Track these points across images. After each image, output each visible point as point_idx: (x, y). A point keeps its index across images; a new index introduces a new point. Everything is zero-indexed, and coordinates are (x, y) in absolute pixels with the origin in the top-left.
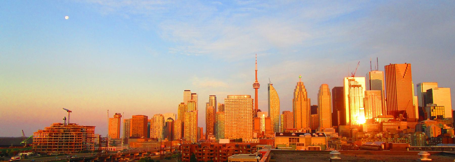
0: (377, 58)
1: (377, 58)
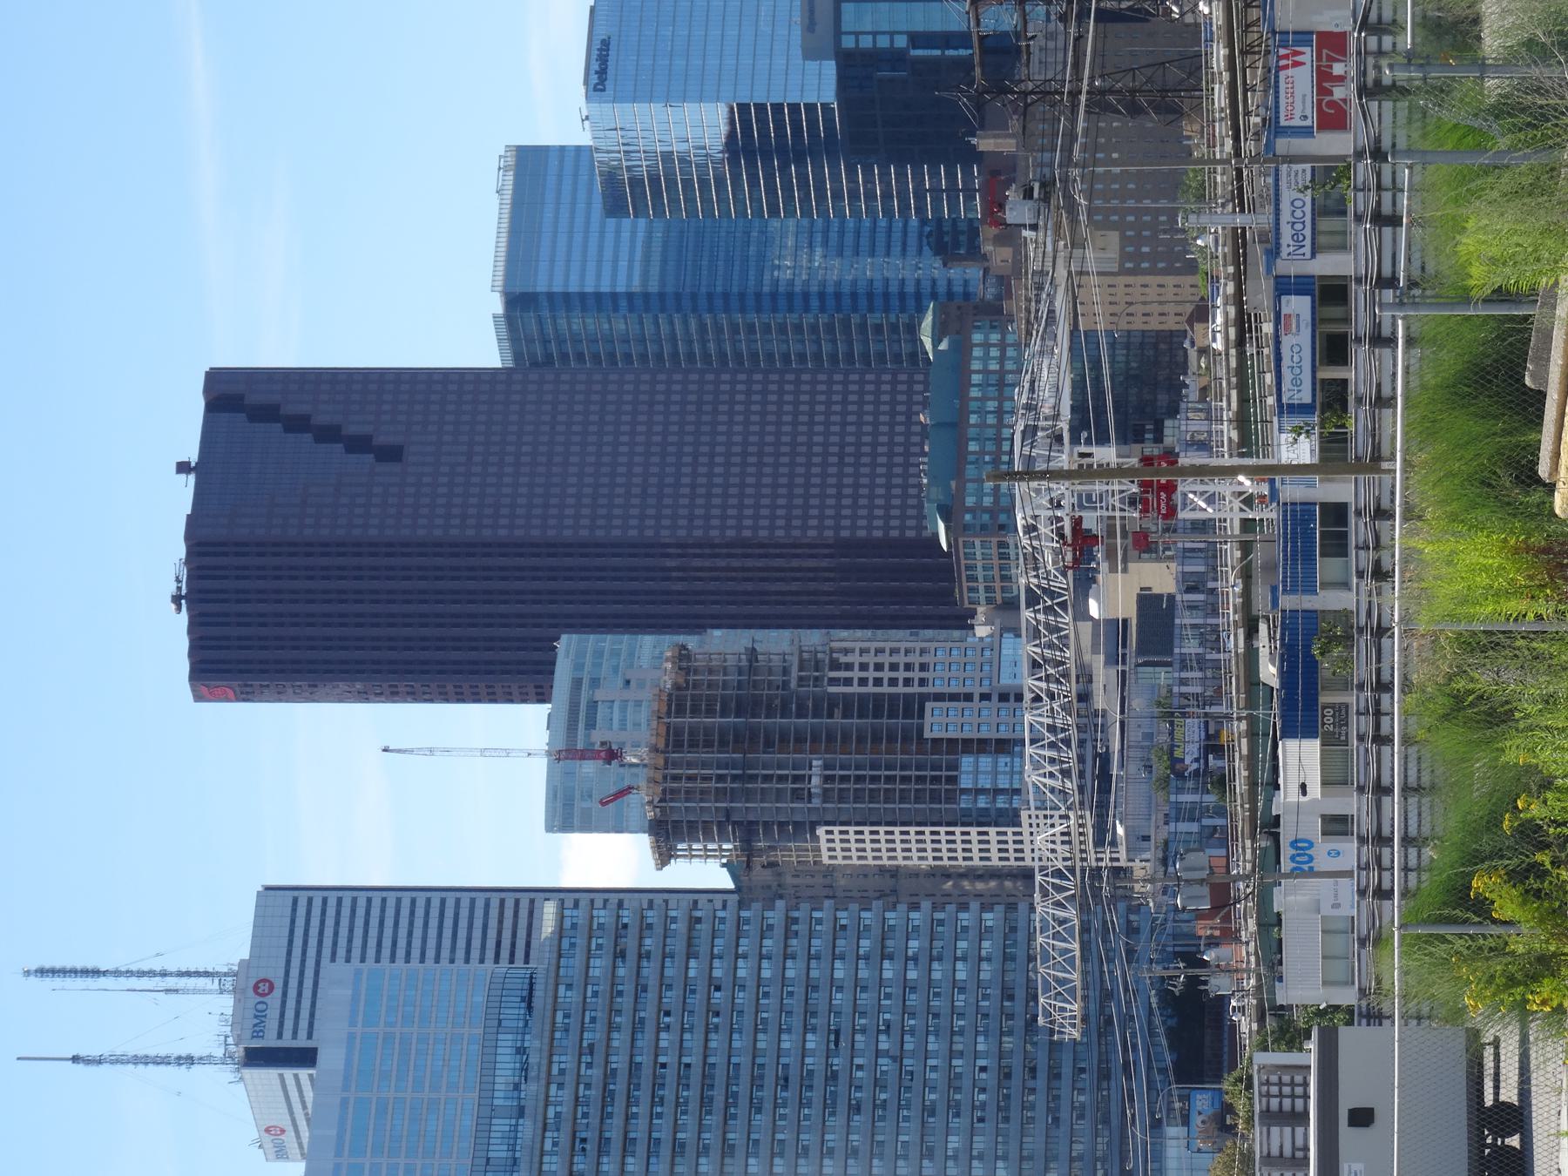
0: (42, 972)
1: (42, 972)
